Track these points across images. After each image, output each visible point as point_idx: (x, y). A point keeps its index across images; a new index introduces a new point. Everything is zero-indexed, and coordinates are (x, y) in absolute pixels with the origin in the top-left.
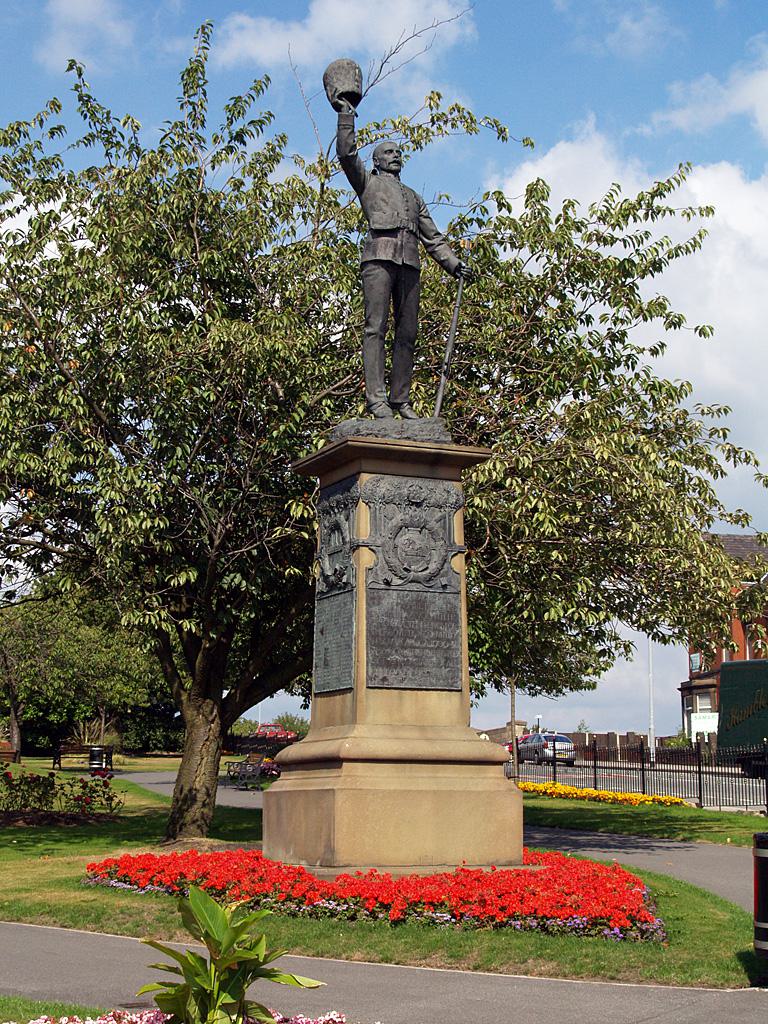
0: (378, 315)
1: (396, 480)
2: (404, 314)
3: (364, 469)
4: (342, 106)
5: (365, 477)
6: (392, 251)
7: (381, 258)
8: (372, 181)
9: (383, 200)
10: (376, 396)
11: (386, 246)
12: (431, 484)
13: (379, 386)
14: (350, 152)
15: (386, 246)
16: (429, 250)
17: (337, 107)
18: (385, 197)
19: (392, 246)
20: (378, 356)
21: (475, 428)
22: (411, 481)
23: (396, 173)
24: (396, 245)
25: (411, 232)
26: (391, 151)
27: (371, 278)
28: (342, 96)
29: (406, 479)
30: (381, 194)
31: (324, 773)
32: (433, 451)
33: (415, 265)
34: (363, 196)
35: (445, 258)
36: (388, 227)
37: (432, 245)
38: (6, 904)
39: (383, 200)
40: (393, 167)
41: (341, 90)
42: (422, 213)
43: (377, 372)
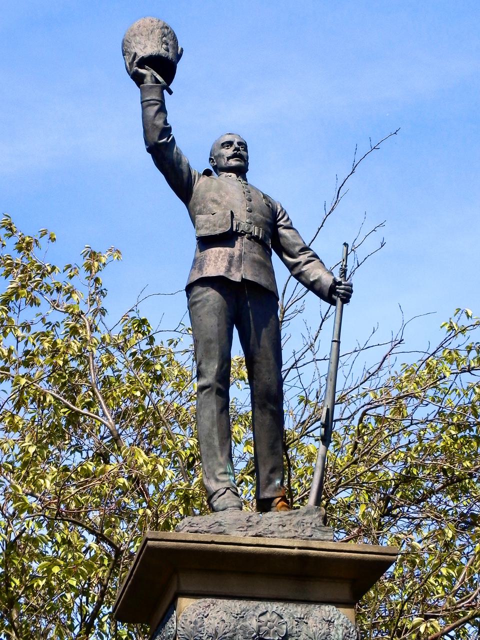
0: (211, 358)
1: (237, 606)
2: (258, 359)
3: (184, 588)
4: (143, 76)
5: (186, 605)
6: (226, 264)
7: (208, 275)
8: (201, 184)
9: (214, 201)
10: (217, 480)
11: (217, 258)
12: (299, 610)
13: (221, 465)
14: (161, 138)
15: (217, 258)
16: (296, 271)
17: (138, 79)
18: (216, 197)
19: (227, 258)
20: (215, 420)
21: (110, 384)
22: (263, 606)
23: (241, 171)
24: (232, 257)
25: (256, 239)
26: (230, 143)
27: (198, 305)
28: (145, 62)
29: (256, 603)
30: (213, 195)
31: (357, 550)
32: (296, 551)
33: (262, 280)
34: (191, 203)
35: (316, 278)
36: (218, 232)
37: (298, 264)
38: (404, 473)
39: (214, 201)
40: (233, 163)
41: (141, 54)
42: (281, 223)
43: (216, 443)
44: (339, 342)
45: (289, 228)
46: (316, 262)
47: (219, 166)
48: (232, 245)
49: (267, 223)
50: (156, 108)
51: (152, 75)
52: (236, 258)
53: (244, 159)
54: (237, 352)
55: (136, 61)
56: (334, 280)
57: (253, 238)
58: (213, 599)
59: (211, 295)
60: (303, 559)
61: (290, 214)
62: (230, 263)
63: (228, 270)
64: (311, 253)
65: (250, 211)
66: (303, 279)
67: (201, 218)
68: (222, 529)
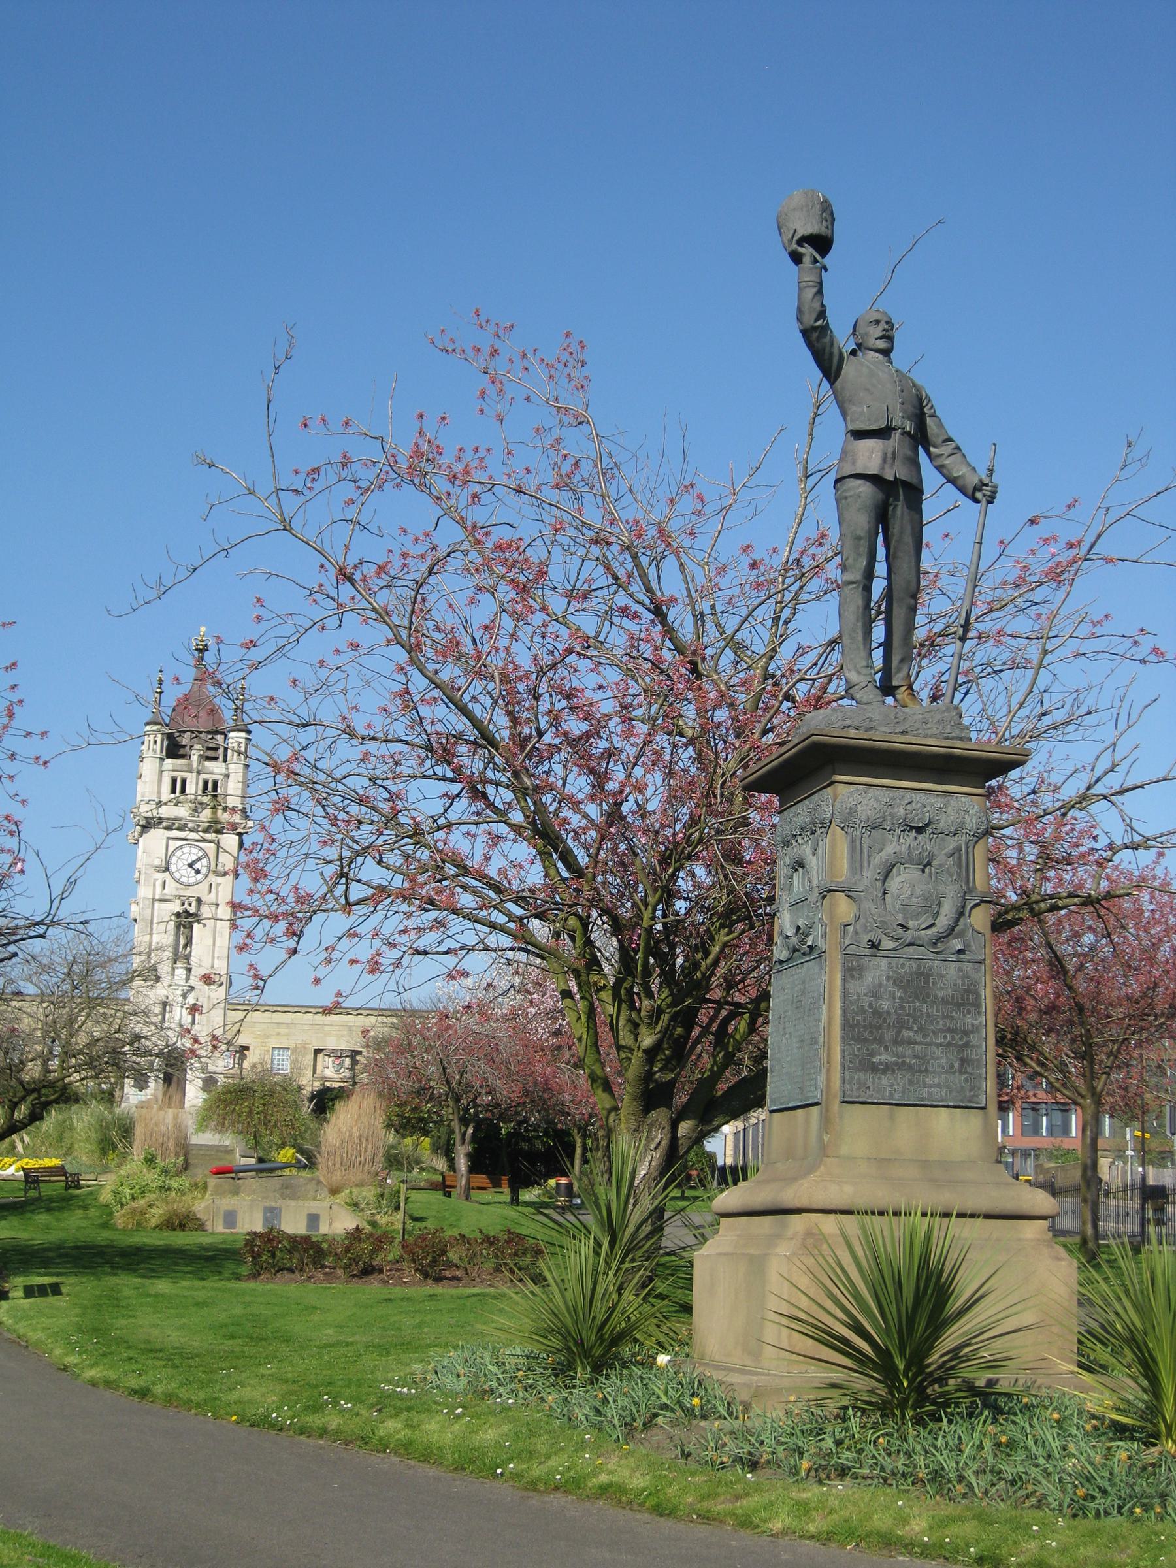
14: (817, 320)
17: (796, 258)
23: (886, 352)
25: (908, 433)
26: (878, 322)
28: (804, 240)
33: (914, 481)
44: (980, 543)
45: (933, 416)
46: (958, 457)
47: (865, 344)
48: (888, 438)
49: (916, 415)
50: (815, 290)
51: (812, 255)
52: (889, 455)
53: (890, 338)
54: (881, 553)
55: (796, 238)
56: (981, 481)
57: (905, 433)
58: (112, 1280)
59: (865, 489)
60: (949, 757)
61: (934, 402)
62: (884, 460)
63: (883, 468)
64: (953, 445)
65: (903, 404)
66: (945, 471)
67: (853, 409)
68: (872, 724)
